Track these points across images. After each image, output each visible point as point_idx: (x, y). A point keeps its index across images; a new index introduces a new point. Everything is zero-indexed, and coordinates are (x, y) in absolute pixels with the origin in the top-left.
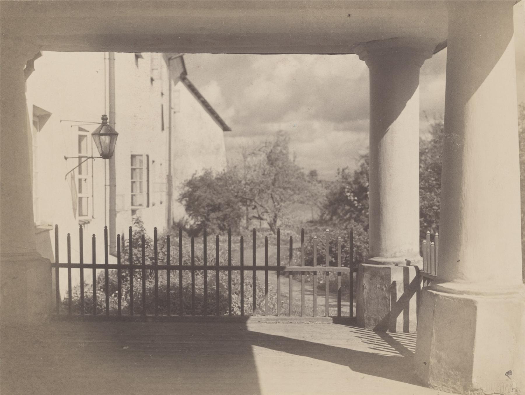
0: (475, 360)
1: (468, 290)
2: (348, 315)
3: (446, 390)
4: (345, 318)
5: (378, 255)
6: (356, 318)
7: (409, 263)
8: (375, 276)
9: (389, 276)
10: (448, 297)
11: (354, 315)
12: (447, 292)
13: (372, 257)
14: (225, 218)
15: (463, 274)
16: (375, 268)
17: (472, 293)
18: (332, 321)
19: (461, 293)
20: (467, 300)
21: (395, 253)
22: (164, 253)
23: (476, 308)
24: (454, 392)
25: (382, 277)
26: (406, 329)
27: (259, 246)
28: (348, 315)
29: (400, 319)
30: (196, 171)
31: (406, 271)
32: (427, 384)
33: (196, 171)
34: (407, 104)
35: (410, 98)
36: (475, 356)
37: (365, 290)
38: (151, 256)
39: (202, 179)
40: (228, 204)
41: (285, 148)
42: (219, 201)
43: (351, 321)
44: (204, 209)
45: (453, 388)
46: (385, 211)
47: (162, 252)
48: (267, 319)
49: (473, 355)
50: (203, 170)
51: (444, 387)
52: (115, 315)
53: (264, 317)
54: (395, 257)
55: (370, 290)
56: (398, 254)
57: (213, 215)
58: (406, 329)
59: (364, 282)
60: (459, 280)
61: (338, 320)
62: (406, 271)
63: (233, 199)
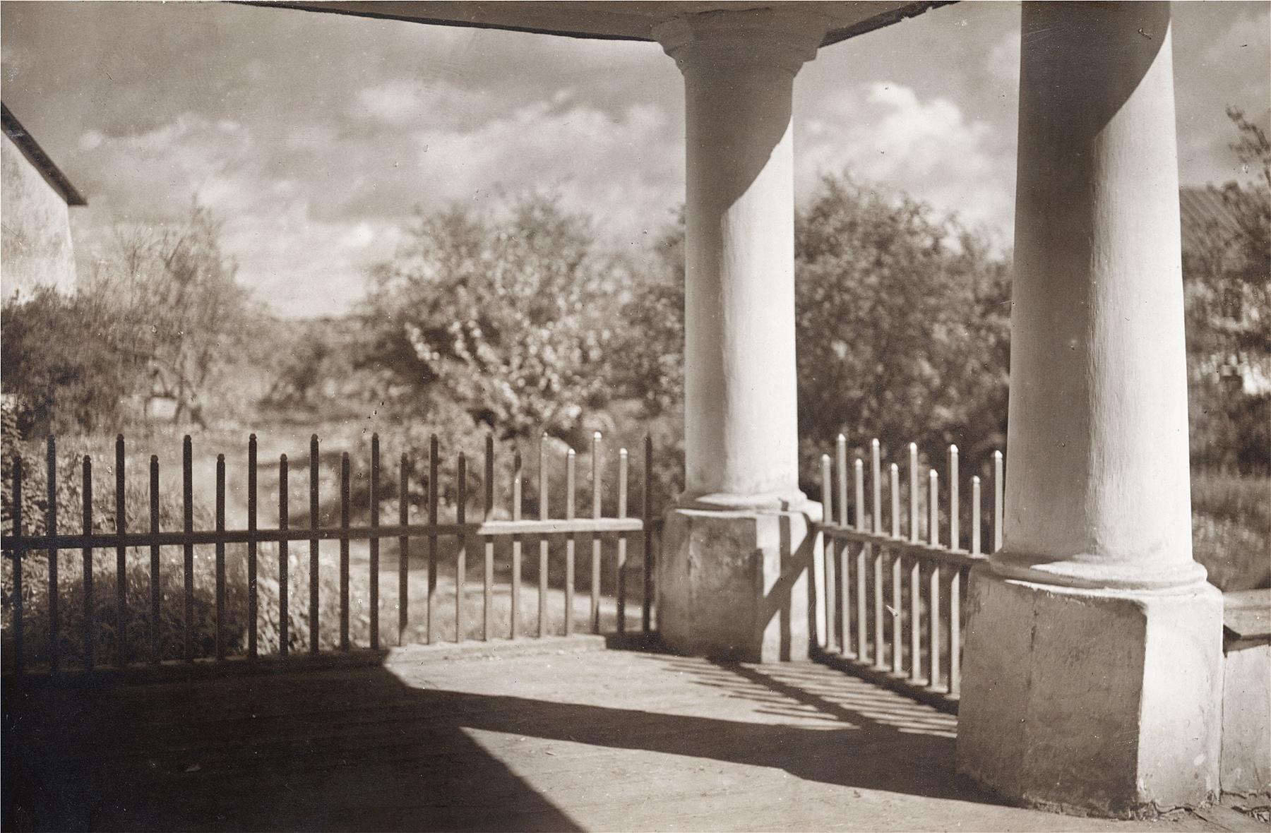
0: (1142, 737)
1: (1115, 578)
2: (638, 628)
3: (1070, 811)
4: (632, 634)
5: (719, 490)
6: (657, 632)
7: (785, 506)
8: (717, 537)
9: (752, 537)
10: (1070, 596)
11: (653, 625)
12: (1068, 585)
13: (704, 494)
14: (88, 399)
15: (1095, 542)
16: (718, 519)
17: (1133, 586)
18: (603, 646)
19: (1101, 585)
20: (1121, 602)
21: (758, 485)
22: (73, 492)
23: (1144, 619)
24: (1090, 815)
25: (735, 542)
26: (785, 656)
27: (201, 456)
28: (638, 628)
29: (772, 633)
30: (17, 292)
31: (785, 523)
32: (1021, 799)
33: (17, 292)
34: (773, 154)
35: (778, 141)
36: (1141, 729)
37: (693, 571)
38: (40, 499)
39: (33, 309)
40: (99, 367)
41: (211, 245)
42: (78, 359)
43: (648, 642)
44: (43, 377)
45: (1090, 806)
46: (733, 392)
47: (69, 488)
48: (465, 651)
49: (1138, 727)
50: (36, 288)
51: (1065, 805)
52: (109, 667)
53: (455, 646)
54: (757, 493)
55: (706, 570)
56: (764, 487)
57: (60, 391)
58: (785, 656)
59: (691, 553)
60: (1085, 556)
61: (621, 640)
62: (785, 523)
63: (108, 355)
